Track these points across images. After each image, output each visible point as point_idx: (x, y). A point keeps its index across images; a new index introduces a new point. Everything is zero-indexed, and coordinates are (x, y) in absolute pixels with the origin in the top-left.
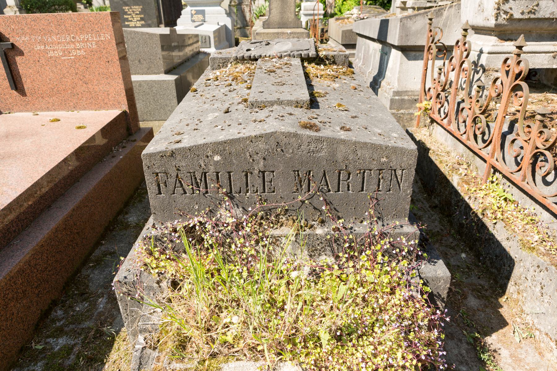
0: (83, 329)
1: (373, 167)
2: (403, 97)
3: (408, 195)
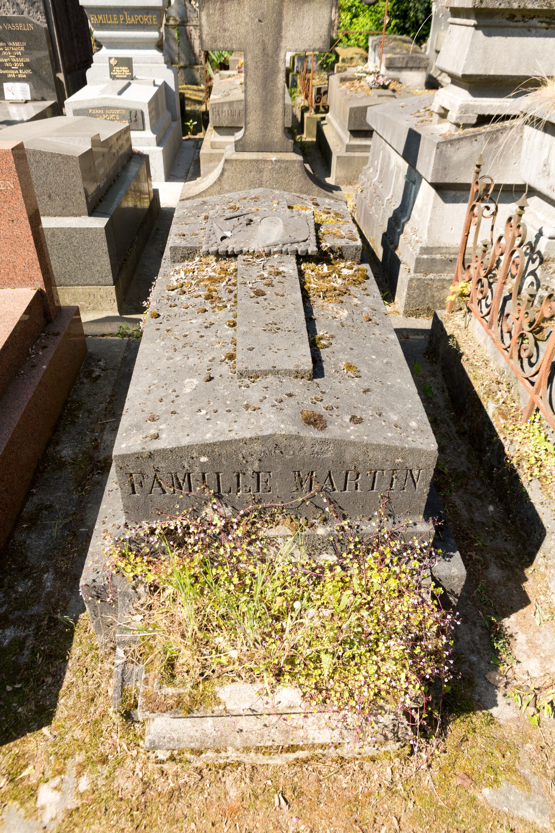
0: (32, 616)
1: (385, 467)
2: (433, 256)
3: (424, 493)
